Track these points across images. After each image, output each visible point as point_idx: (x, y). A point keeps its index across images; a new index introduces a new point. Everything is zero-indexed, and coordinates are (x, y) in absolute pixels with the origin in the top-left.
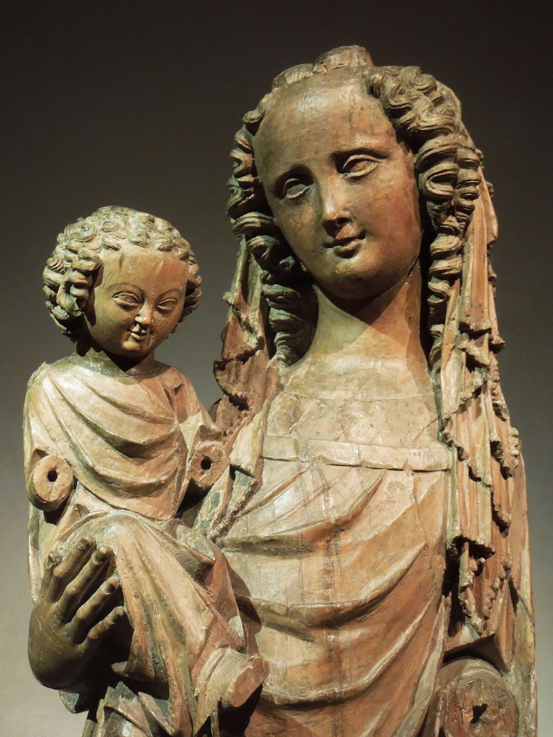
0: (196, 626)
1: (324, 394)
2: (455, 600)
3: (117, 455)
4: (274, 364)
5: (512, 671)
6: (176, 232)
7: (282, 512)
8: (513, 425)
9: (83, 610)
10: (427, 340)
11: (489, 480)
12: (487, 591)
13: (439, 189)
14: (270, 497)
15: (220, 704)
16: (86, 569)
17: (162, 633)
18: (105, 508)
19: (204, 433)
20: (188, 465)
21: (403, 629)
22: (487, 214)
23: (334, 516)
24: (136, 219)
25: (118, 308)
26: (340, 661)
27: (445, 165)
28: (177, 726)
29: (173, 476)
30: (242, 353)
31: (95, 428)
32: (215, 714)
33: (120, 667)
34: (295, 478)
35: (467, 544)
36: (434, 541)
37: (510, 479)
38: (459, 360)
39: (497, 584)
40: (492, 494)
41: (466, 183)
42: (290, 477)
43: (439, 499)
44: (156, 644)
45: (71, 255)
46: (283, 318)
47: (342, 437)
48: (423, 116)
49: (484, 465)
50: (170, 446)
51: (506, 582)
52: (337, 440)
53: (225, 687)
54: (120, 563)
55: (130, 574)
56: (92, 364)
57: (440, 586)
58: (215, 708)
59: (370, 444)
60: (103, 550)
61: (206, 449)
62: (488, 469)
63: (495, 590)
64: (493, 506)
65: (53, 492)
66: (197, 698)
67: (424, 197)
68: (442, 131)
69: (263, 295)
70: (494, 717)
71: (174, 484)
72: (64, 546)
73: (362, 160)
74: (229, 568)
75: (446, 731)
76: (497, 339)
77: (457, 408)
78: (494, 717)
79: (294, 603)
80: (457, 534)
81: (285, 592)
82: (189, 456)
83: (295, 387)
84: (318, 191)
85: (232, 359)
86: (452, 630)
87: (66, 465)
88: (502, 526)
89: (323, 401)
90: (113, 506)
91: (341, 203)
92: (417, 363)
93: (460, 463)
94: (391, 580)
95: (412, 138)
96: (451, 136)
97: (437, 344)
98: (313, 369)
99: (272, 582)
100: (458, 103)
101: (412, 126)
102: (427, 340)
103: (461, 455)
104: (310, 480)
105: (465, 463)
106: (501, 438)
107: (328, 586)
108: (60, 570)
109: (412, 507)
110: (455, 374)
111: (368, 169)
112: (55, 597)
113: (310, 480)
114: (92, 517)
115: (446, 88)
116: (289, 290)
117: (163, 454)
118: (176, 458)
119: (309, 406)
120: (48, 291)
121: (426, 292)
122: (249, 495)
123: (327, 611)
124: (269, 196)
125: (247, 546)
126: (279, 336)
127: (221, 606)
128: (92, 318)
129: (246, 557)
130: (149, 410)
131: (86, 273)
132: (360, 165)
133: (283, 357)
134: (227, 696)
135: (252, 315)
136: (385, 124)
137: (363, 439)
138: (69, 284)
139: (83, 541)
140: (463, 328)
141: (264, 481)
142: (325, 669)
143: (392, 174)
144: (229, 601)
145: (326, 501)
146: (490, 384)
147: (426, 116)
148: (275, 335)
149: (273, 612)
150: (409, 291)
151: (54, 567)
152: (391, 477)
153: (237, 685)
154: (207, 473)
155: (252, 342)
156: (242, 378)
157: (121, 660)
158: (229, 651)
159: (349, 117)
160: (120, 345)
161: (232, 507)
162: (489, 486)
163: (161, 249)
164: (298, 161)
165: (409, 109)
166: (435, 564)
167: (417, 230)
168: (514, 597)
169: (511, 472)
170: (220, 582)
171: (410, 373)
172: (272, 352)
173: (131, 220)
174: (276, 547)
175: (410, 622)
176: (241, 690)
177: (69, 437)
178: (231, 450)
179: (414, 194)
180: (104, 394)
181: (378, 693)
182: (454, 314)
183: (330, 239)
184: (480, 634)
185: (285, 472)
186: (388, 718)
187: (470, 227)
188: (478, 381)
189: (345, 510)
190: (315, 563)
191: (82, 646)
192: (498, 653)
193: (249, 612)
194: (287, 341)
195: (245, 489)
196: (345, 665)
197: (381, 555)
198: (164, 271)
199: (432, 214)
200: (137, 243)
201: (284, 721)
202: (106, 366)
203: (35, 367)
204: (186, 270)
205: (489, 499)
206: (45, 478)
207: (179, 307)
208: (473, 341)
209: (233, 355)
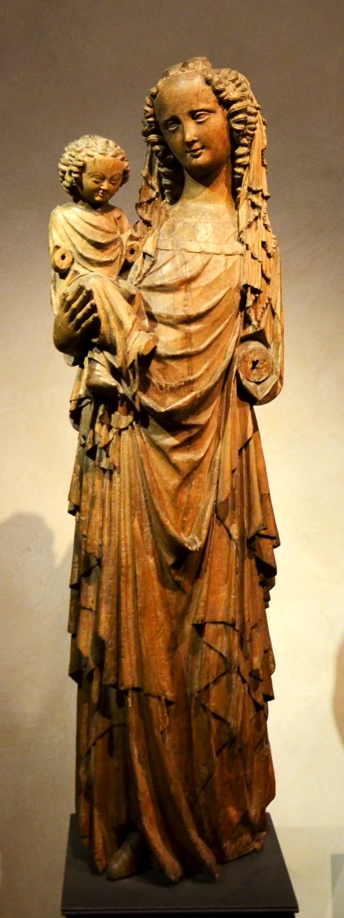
0: (128, 322)
1: (186, 220)
2: (246, 314)
3: (93, 248)
4: (164, 205)
5: (272, 347)
6: (119, 147)
7: (166, 274)
8: (273, 234)
9: (79, 315)
10: (234, 195)
11: (260, 259)
12: (260, 311)
13: (238, 127)
14: (161, 267)
15: (138, 354)
16: (81, 297)
17: (114, 324)
18: (87, 272)
19: (131, 238)
20: (124, 252)
21: (220, 325)
22: (262, 136)
23: (189, 275)
24: (101, 141)
25: (93, 183)
26: (191, 339)
27: (241, 116)
28: (120, 364)
29: (117, 258)
30: (148, 199)
31: (82, 236)
32: (136, 358)
33: (95, 340)
34: (172, 258)
35: (249, 289)
36: (234, 286)
37: (272, 259)
38: (247, 204)
39: (265, 306)
40: (262, 266)
41: (251, 123)
42: (170, 258)
43: (237, 268)
44: (111, 329)
45: (72, 158)
46: (168, 183)
47: (194, 239)
48: (231, 93)
49: (258, 252)
50: (116, 244)
51: (269, 306)
52: (191, 241)
53: (141, 346)
54: (95, 295)
55: (99, 299)
56: (80, 207)
57: (238, 307)
58: (136, 356)
59: (206, 242)
60: (88, 289)
61: (132, 245)
62: (260, 254)
63: (264, 309)
64: (262, 271)
65: (63, 265)
66: (128, 352)
67: (231, 130)
68: (240, 100)
69: (159, 172)
70: (261, 366)
71: (118, 261)
72: (69, 288)
73: (202, 114)
74: (143, 298)
75: (239, 371)
76: (266, 193)
77: (246, 226)
78: (261, 366)
79: (171, 313)
80: (245, 283)
81: (167, 309)
82: (124, 248)
83: (173, 216)
84: (183, 128)
85: (144, 203)
86: (245, 328)
87: (70, 253)
88: (268, 281)
89: (185, 223)
90: (91, 271)
91: (193, 133)
92: (230, 205)
93: (247, 251)
94: (214, 304)
95: (226, 104)
96: (244, 102)
97: (239, 196)
98: (181, 208)
99: (161, 304)
100: (249, 84)
101: (225, 98)
102: (234, 195)
103: (247, 247)
104: (178, 260)
105: (249, 251)
106: (267, 240)
107: (186, 306)
108: (69, 298)
109: (225, 271)
110: (246, 210)
111: (205, 118)
112: (66, 310)
113: (178, 260)
114: (81, 276)
115: (244, 77)
116: (171, 170)
117: (113, 247)
118: (119, 249)
119: (179, 225)
120: (61, 174)
121: (234, 173)
122: (152, 266)
123: (185, 316)
124: (161, 128)
125: (151, 289)
126: (166, 191)
127: (138, 313)
128: (82, 186)
129: (150, 293)
130: (107, 228)
131: (79, 167)
132: (202, 116)
133: (168, 201)
134: (141, 351)
135: (154, 182)
136: (213, 97)
137: (203, 240)
138: (71, 172)
139: (80, 285)
140: (250, 189)
141: (158, 259)
142: (184, 341)
143: (217, 120)
144: (142, 312)
145: (186, 268)
146: (262, 215)
147: (232, 93)
148: (164, 191)
149: (161, 317)
150: (226, 172)
151: (66, 297)
152: (215, 257)
153: (145, 346)
154: (132, 256)
155: (154, 194)
156: (149, 211)
157: (96, 337)
158: (142, 332)
159: (197, 95)
160: (94, 198)
161: (144, 271)
162: (260, 262)
163: (112, 156)
164: (174, 114)
165: (224, 91)
166: (235, 297)
167: (228, 144)
168: (274, 314)
169: (272, 255)
170: (139, 303)
171: (226, 209)
172: (163, 198)
173: (98, 142)
174: (163, 289)
175: (223, 322)
176: (147, 348)
177: (71, 240)
178: (143, 246)
179: (227, 128)
180: (86, 221)
181: (208, 353)
182: (246, 183)
183: (188, 149)
184: (256, 329)
185: (168, 255)
186: (212, 364)
187: (253, 143)
188: (257, 214)
189: (194, 272)
190: (180, 296)
191: (78, 332)
192: (265, 338)
193: (151, 317)
194: (169, 193)
195: (150, 263)
196: (193, 340)
197: (210, 292)
198: (113, 166)
199: (235, 137)
200: (101, 154)
201: (166, 364)
202: (87, 208)
203: (54, 207)
204: (123, 165)
205: (260, 267)
206: (60, 258)
207: (120, 181)
208: (254, 195)
209: (145, 200)
